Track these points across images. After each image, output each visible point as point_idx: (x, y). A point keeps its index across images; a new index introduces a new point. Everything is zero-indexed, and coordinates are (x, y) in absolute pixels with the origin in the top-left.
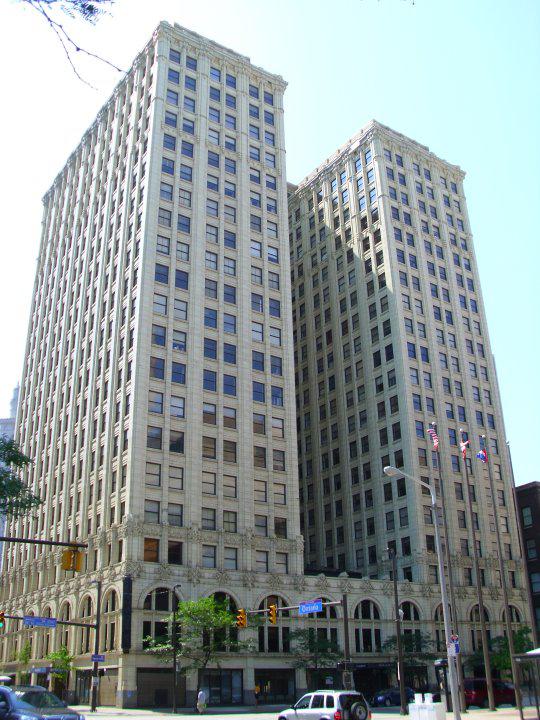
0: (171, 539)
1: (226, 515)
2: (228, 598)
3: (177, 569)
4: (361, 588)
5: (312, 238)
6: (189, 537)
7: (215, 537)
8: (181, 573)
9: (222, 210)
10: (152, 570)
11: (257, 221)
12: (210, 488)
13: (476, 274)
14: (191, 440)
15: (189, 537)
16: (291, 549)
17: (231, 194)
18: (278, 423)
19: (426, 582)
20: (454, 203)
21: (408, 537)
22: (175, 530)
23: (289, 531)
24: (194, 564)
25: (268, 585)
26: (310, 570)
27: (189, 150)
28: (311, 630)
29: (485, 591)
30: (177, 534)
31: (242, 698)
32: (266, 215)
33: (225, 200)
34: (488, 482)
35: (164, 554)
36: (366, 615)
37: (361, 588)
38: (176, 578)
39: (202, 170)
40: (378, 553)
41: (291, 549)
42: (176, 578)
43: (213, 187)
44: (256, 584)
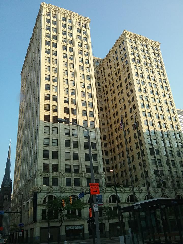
0: (53, 177)
1: (75, 166)
2: (54, 198)
3: (55, 188)
4: (129, 190)
5: (108, 75)
6: (81, 176)
7: (70, 175)
8: (57, 189)
9: (69, 65)
10: (46, 189)
11: (82, 67)
12: (69, 158)
13: (115, 47)
14: (80, 144)
15: (81, 176)
16: (180, 180)
17: (72, 59)
18: (93, 134)
19: (39, 185)
20: (158, 61)
21: (147, 171)
22: (55, 174)
23: (99, 170)
24: (84, 186)
25: (71, 191)
26: (108, 185)
27: (55, 45)
28: (110, 208)
29: (151, 189)
30: (77, 175)
31: (84, 236)
32: (85, 65)
33: (70, 61)
34: (150, 140)
35: (51, 182)
36: (114, 201)
37: (129, 190)
38: (56, 191)
39: (61, 52)
40: (138, 178)
41: (100, 177)
42: (56, 191)
43: (65, 57)
44: (65, 191)
